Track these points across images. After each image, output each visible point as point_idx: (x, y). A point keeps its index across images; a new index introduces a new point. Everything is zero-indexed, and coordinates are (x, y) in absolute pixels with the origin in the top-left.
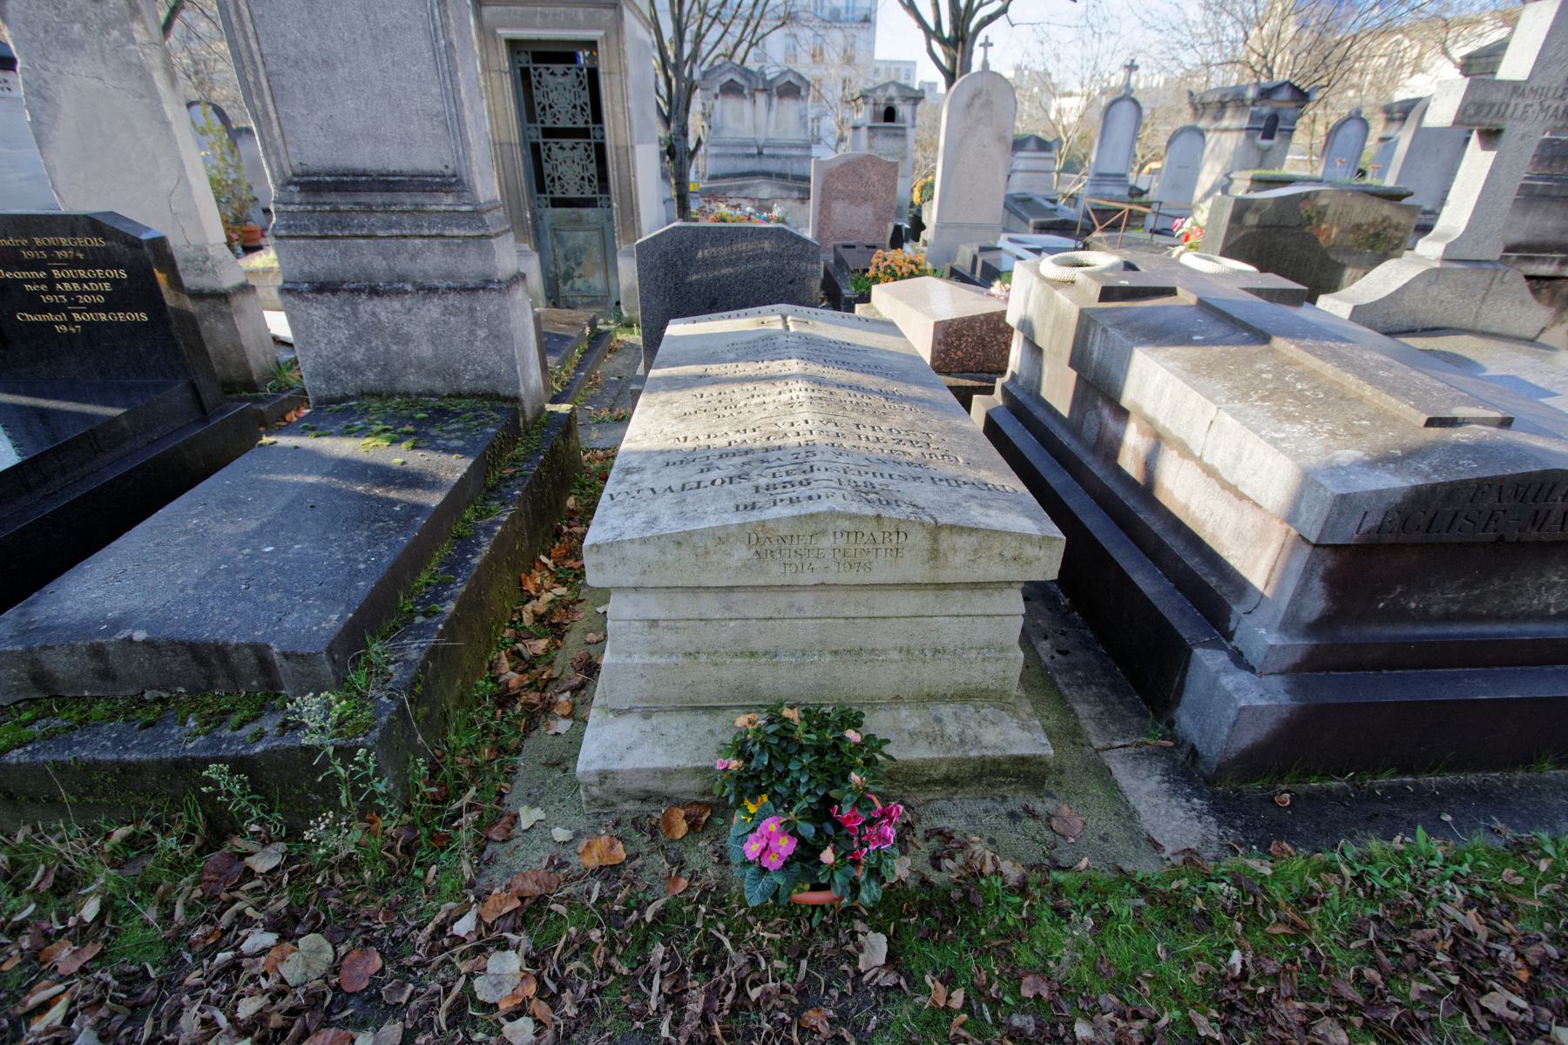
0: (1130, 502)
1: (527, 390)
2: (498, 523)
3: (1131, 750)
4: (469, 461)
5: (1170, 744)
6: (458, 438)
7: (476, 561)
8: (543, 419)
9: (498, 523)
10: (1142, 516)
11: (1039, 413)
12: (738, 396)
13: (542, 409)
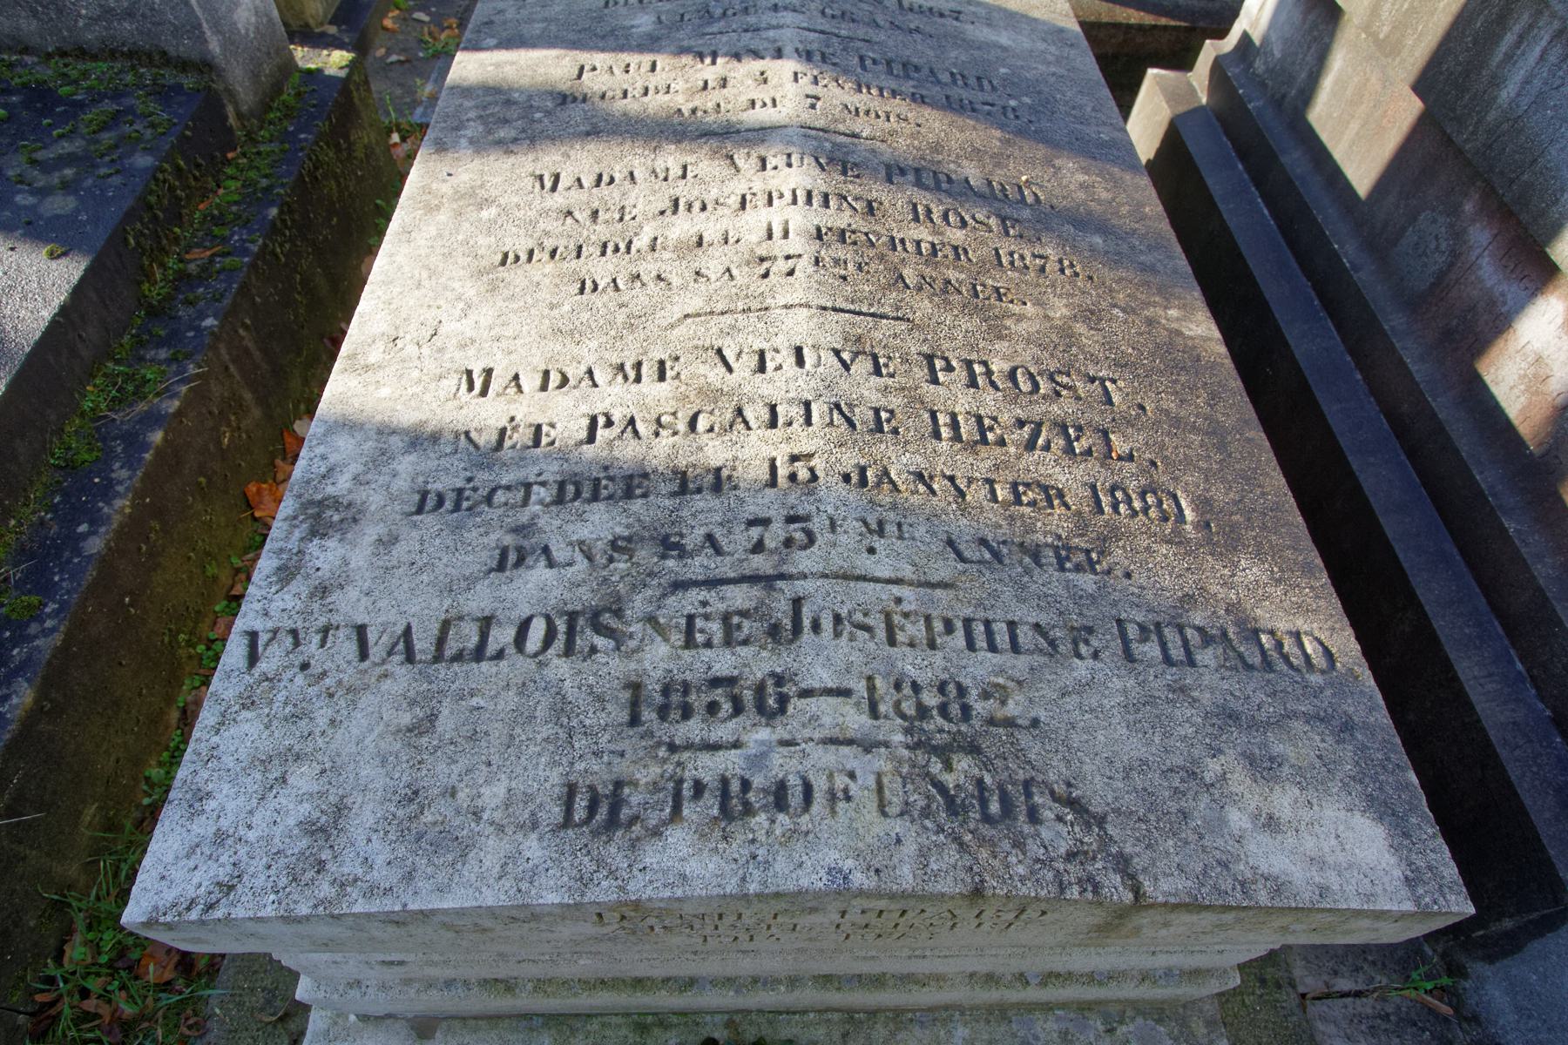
0: (1486, 477)
1: (231, 41)
2: (153, 419)
3: (1367, 1006)
4: (71, 270)
5: (1445, 1009)
6: (67, 187)
7: (95, 545)
8: (287, 96)
9: (153, 419)
10: (1511, 526)
11: (1293, 160)
12: (644, 199)
13: (289, 65)
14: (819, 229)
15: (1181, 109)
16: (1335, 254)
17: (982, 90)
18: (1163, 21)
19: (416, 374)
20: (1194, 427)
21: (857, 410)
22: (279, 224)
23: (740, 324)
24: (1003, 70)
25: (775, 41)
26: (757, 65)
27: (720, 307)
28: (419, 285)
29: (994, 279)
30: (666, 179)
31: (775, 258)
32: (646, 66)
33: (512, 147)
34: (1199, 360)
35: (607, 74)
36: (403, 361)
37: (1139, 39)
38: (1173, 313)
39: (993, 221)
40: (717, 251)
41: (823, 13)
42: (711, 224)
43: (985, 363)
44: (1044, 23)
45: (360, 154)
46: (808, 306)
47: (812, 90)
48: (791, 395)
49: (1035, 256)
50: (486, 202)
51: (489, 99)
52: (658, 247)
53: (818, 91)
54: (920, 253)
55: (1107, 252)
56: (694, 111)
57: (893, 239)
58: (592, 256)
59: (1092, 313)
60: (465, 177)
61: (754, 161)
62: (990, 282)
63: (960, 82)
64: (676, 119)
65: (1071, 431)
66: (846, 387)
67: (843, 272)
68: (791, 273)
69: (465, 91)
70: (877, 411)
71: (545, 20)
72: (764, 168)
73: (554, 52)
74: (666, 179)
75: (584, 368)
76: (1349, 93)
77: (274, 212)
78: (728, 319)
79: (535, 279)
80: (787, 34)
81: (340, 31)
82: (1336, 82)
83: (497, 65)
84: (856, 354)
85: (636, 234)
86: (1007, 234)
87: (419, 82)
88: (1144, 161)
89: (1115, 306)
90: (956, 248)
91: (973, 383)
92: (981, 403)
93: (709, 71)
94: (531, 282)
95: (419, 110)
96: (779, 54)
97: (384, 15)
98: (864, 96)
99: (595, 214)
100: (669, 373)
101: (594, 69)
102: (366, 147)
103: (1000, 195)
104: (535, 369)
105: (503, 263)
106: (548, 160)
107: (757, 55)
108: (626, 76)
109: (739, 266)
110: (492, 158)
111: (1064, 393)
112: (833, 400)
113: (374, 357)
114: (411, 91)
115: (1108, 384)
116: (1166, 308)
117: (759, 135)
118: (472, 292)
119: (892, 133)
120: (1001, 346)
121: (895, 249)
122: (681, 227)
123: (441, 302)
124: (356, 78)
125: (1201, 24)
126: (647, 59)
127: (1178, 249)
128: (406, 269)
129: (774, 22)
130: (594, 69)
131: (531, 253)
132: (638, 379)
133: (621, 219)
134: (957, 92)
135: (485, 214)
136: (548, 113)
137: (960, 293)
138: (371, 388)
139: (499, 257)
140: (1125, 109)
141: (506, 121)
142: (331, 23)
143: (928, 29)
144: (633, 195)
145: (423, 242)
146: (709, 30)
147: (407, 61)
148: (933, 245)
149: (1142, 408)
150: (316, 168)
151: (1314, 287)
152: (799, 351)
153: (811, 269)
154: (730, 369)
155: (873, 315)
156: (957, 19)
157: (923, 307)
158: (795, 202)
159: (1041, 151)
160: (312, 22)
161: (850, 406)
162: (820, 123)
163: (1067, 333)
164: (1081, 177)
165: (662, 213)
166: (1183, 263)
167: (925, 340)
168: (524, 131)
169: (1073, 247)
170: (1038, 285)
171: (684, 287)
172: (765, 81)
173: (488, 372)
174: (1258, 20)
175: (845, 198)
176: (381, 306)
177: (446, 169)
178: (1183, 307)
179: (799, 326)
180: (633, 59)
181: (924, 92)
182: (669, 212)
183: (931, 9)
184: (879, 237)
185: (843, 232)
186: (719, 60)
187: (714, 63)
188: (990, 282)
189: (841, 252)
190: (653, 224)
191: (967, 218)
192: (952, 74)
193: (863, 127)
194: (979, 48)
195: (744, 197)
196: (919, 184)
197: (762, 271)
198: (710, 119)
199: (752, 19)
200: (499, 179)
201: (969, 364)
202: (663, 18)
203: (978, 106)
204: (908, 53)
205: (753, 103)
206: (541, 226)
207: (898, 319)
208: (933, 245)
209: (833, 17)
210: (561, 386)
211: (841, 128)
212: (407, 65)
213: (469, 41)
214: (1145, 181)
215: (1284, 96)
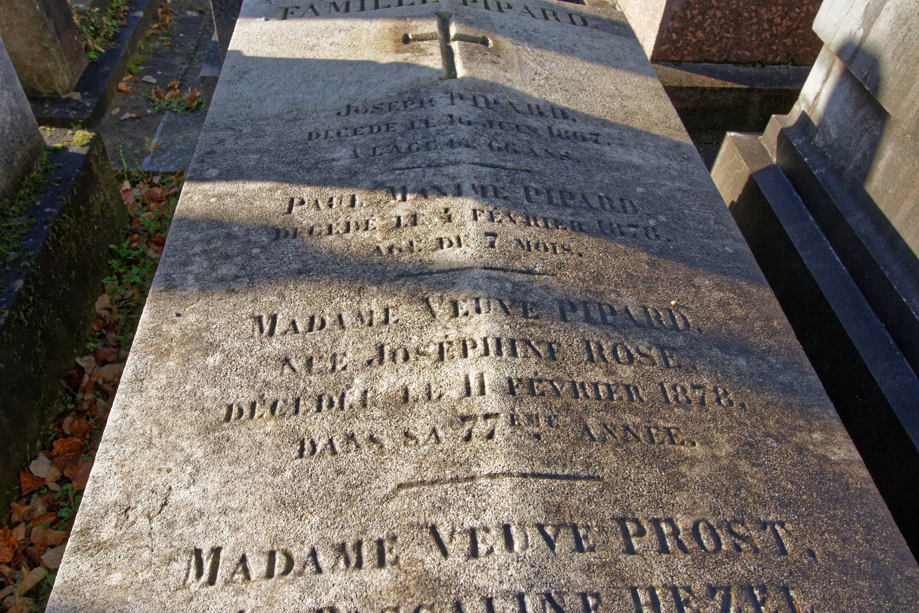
8: (38, 168)
11: (856, 219)
12: (352, 348)
13: (39, 147)
14: (510, 381)
15: (758, 167)
16: (904, 305)
17: (625, 212)
18: (729, 85)
19: (146, 554)
20: (859, 570)
21: (566, 599)
22: (23, 293)
23: (452, 496)
24: (640, 190)
25: (454, 178)
26: (441, 203)
27: (430, 475)
28: (150, 445)
29: (664, 419)
30: (370, 324)
31: (475, 418)
32: (346, 203)
33: (234, 286)
34: (848, 489)
35: (316, 208)
36: (134, 538)
37: (712, 97)
38: (816, 436)
39: (654, 353)
40: (423, 408)
41: (490, 145)
42: (415, 377)
43: (670, 521)
44: (664, 139)
45: (96, 211)
46: (509, 474)
47: (488, 227)
48: (505, 587)
49: (694, 387)
50: (211, 348)
51: (212, 232)
52: (369, 403)
53: (495, 227)
54: (598, 397)
55: (752, 375)
56: (391, 249)
57: (574, 383)
58: (306, 394)
59: (751, 445)
60: (192, 318)
61: (447, 306)
62: (661, 423)
63: (607, 206)
64: (376, 259)
65: (756, 592)
66: (553, 571)
67: (536, 430)
68: (491, 436)
69: (191, 224)
70: (584, 596)
71: (259, 151)
72: (456, 314)
73: (267, 185)
74: (370, 324)
75: (307, 550)
76: (901, 177)
77: (20, 283)
78: (438, 491)
79: (258, 438)
80: (464, 169)
81: (83, 97)
82: (889, 166)
83: (219, 197)
84: (557, 528)
85: (348, 387)
86: (668, 366)
87: (147, 139)
88: (727, 201)
89: (768, 435)
90: (627, 387)
91: (664, 549)
92: (675, 573)
93: (401, 208)
94: (254, 441)
95: (147, 159)
96: (459, 192)
97: (119, 79)
98: (533, 229)
99: (309, 361)
100: (389, 557)
101: (302, 202)
102: (102, 205)
103: (656, 323)
104: (260, 552)
105: (228, 418)
106: (266, 301)
107: (442, 193)
108: (330, 212)
109: (443, 427)
110: (216, 297)
111: (743, 546)
112: (544, 590)
113: (107, 532)
114: (140, 143)
115: (777, 527)
116: (811, 431)
117: (448, 278)
118: (199, 453)
119: (560, 266)
120: (681, 498)
121: (577, 397)
122: (388, 381)
123: (171, 465)
124: (95, 152)
125: (758, 86)
126: (347, 193)
127: (807, 363)
128: (139, 424)
129: (452, 158)
130: (302, 202)
131: (253, 406)
132: (359, 565)
133: (334, 368)
134: (608, 217)
135: (211, 361)
136: (264, 249)
137: (637, 439)
138: (103, 573)
139: (224, 411)
140: (709, 162)
141: (227, 257)
142: (76, 90)
143: (575, 154)
144: (343, 341)
145: (153, 393)
146: (398, 165)
147: (137, 117)
148: (608, 386)
149: (811, 553)
150: (59, 236)
151: (888, 327)
152: (506, 529)
153: (508, 431)
154: (445, 553)
155: (567, 477)
156: (596, 141)
157: (609, 460)
158: (487, 353)
159: (682, 271)
160: (59, 91)
161: (560, 594)
162: (500, 263)
163: (733, 473)
164: (718, 295)
165: (370, 362)
166: (813, 378)
167: (616, 500)
168: (243, 268)
169: (723, 372)
170: (701, 421)
171: (396, 451)
172: (449, 219)
173: (216, 551)
174: (814, 105)
175: (529, 343)
176: (114, 468)
177: (175, 310)
178: (823, 429)
179: (502, 500)
180: (336, 193)
181: (581, 220)
182: (375, 362)
183: (575, 134)
184: (562, 382)
185: (531, 381)
186: (409, 197)
187: (404, 199)
188: (661, 423)
189: (533, 407)
190: (363, 376)
191: (632, 351)
192: (600, 197)
193: (535, 262)
194: (618, 169)
195: (441, 345)
196: (588, 319)
197: (465, 434)
198: (406, 257)
199: (433, 155)
200: (222, 321)
201: (656, 523)
202: (358, 151)
203: (624, 230)
204: (562, 180)
205: (440, 241)
206: (262, 375)
207: (588, 478)
208: (608, 386)
209: (499, 149)
210: (286, 572)
211: (518, 265)
212: (137, 121)
213: (194, 170)
214: (729, 214)
215: (843, 168)
